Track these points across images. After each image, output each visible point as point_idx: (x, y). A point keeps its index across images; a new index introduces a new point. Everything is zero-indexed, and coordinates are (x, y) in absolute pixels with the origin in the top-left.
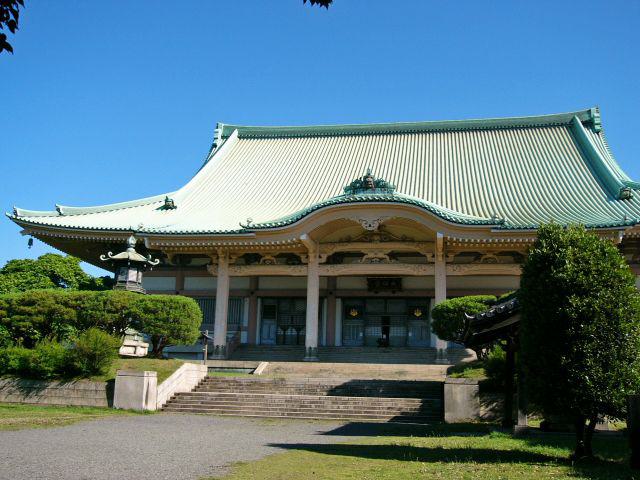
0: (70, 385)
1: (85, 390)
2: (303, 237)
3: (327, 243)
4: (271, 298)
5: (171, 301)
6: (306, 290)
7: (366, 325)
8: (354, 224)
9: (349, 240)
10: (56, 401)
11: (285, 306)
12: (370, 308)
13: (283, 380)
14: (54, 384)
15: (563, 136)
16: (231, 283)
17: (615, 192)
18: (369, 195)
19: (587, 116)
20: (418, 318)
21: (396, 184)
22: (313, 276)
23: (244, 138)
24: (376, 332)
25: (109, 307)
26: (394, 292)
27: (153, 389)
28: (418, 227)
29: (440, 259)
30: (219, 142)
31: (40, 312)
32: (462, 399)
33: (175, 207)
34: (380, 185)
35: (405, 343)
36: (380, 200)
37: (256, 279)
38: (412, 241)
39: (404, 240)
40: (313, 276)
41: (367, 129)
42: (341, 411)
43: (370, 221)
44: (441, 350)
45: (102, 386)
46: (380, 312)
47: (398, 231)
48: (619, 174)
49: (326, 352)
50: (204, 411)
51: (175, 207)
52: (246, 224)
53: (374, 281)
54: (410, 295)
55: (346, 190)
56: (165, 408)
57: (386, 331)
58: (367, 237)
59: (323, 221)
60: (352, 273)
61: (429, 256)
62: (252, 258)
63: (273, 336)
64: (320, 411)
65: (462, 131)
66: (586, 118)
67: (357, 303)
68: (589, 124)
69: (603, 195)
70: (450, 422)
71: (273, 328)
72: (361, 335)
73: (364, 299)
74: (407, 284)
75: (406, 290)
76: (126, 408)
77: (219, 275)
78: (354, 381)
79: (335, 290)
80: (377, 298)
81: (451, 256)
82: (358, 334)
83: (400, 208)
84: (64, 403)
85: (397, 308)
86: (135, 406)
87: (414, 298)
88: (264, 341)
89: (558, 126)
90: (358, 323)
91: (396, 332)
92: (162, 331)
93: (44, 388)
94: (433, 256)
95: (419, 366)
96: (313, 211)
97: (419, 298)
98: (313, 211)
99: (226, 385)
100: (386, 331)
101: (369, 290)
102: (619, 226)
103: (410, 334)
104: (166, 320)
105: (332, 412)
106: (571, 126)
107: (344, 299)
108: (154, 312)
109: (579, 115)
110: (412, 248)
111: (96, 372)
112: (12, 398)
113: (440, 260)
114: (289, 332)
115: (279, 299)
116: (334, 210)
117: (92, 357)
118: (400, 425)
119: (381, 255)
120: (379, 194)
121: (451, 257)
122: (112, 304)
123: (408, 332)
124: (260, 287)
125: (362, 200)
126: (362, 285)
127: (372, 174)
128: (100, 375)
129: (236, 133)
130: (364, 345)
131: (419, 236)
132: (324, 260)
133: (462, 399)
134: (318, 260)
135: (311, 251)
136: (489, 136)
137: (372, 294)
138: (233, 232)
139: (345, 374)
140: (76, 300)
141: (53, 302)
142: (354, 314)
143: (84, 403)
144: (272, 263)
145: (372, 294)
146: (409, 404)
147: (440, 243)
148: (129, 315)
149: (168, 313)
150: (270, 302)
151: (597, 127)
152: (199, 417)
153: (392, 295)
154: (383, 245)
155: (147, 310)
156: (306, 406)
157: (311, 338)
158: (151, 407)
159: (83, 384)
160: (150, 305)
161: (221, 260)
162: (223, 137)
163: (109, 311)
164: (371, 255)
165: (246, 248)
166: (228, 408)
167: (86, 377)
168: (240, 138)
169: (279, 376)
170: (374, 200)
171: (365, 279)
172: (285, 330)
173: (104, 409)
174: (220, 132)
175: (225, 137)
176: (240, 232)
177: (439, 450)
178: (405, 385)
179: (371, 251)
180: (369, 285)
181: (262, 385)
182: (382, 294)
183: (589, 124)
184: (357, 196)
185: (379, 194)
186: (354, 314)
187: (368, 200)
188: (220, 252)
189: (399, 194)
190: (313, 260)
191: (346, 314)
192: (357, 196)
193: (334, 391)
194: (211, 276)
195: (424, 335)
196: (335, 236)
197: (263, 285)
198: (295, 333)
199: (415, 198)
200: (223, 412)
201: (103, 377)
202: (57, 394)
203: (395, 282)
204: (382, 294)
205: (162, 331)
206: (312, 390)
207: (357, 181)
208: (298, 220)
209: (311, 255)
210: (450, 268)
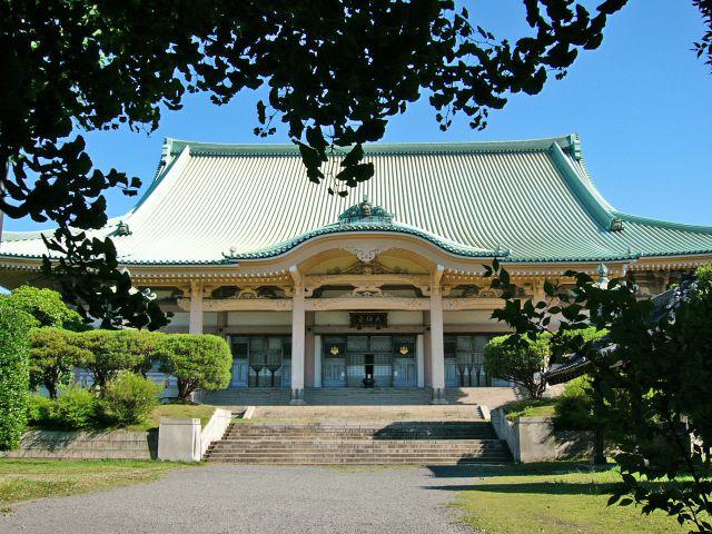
0: (99, 437)
1: (123, 442)
2: (293, 269)
3: (314, 275)
4: (243, 335)
5: (204, 340)
6: (290, 326)
7: (349, 363)
8: (344, 253)
9: (338, 272)
10: (87, 455)
11: (257, 344)
12: (351, 345)
13: (318, 424)
14: (83, 435)
15: (543, 161)
16: (204, 317)
17: (607, 225)
18: (365, 223)
19: (566, 142)
20: (335, 356)
21: (393, 211)
22: (297, 310)
23: (196, 155)
24: (358, 371)
25: (134, 348)
26: (359, 328)
27: (198, 432)
28: (412, 256)
29: (437, 292)
30: (168, 160)
31: (50, 355)
32: (534, 437)
33: (130, 233)
34: (377, 213)
35: (391, 383)
36: (378, 229)
37: (225, 314)
38: (406, 273)
39: (397, 272)
40: (297, 310)
41: (279, 150)
42: (402, 456)
43: (366, 253)
44: (297, 390)
45: (143, 436)
46: (367, 349)
47: (391, 263)
48: (608, 207)
49: (311, 396)
50: (253, 461)
51: (130, 233)
52: (229, 255)
53: (358, 317)
54: (396, 331)
55: (341, 218)
56: (208, 456)
57: (369, 370)
58: (358, 268)
59: (314, 251)
60: (253, 308)
61: (287, 291)
62: (226, 292)
63: (244, 377)
64: (380, 456)
65: (429, 155)
66: (566, 144)
67: (338, 340)
68: (569, 151)
69: (594, 228)
70: (527, 462)
71: (244, 368)
72: (343, 374)
73: (345, 336)
74: (393, 320)
75: (390, 326)
76: (172, 459)
77: (192, 311)
78: (395, 424)
79: (226, 326)
80: (380, 334)
81: (448, 289)
82: (339, 373)
83: (397, 238)
84: (98, 456)
85: (382, 345)
86: (183, 456)
87: (397, 335)
88: (234, 384)
89: (537, 151)
90: (340, 362)
91: (380, 371)
92: (196, 374)
93: (74, 440)
94: (429, 290)
95: (421, 407)
96: (299, 243)
97: (403, 335)
98: (324, 233)
99: (257, 432)
100: (369, 370)
101: (352, 326)
102: (623, 259)
103: (396, 373)
104: (200, 362)
105: (392, 456)
106: (550, 152)
107: (323, 336)
108: (187, 353)
109: (559, 141)
110: (406, 281)
111: (131, 420)
112: (34, 453)
113: (436, 294)
114: (262, 373)
115: (251, 336)
116: (323, 240)
117: (130, 405)
118: (465, 467)
119: (373, 289)
120: (376, 223)
121: (448, 291)
122: (137, 344)
123: (393, 371)
124: (229, 323)
125: (358, 229)
126: (344, 320)
127: (370, 201)
128: (138, 423)
129: (187, 150)
130: (347, 386)
131: (413, 268)
132: (310, 293)
133: (534, 437)
134: (201, 295)
135: (297, 283)
136: (467, 161)
137: (354, 330)
138: (214, 263)
139: (343, 418)
140: (93, 340)
141: (64, 343)
142: (335, 351)
143: (122, 456)
144: (252, 297)
145: (354, 330)
146: (473, 447)
147: (439, 275)
148: (157, 357)
149: (202, 354)
150: (241, 340)
151: (577, 155)
152: (250, 466)
153: (377, 331)
154: (376, 277)
155: (178, 351)
156: (362, 451)
157: (297, 381)
158: (197, 458)
159: (119, 435)
160: (182, 346)
161: (194, 294)
162: (172, 154)
163: (134, 353)
164: (361, 289)
165: (223, 281)
166: (280, 456)
167: (122, 427)
168: (192, 155)
169: (316, 420)
170: (372, 229)
171: (348, 314)
172: (257, 371)
173: (147, 461)
174: (169, 147)
175: (176, 154)
176: (223, 262)
177: (547, 484)
178: (467, 426)
179: (362, 283)
180: (352, 320)
181: (298, 430)
182: (366, 330)
183: (569, 151)
184: (353, 225)
185: (376, 223)
186: (335, 351)
187: (365, 229)
188: (193, 284)
189: (397, 223)
190: (299, 294)
191: (326, 352)
192: (353, 225)
193: (378, 435)
194: (183, 311)
195: (410, 376)
196: (322, 268)
197: (232, 321)
198: (269, 373)
199: (408, 226)
200: (275, 460)
201: (142, 427)
202: (84, 446)
203: (380, 317)
204: (366, 330)
205: (196, 374)
206: (355, 434)
207: (351, 209)
208: (288, 249)
209: (297, 288)
210: (446, 302)
